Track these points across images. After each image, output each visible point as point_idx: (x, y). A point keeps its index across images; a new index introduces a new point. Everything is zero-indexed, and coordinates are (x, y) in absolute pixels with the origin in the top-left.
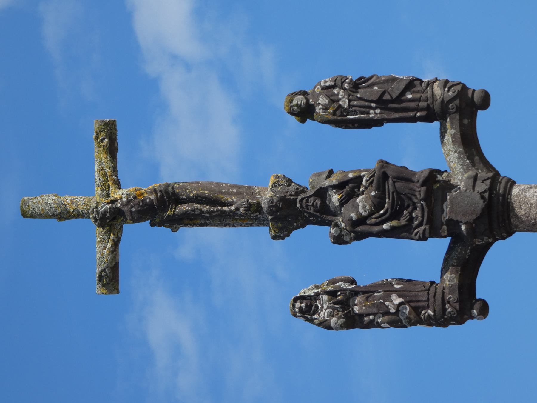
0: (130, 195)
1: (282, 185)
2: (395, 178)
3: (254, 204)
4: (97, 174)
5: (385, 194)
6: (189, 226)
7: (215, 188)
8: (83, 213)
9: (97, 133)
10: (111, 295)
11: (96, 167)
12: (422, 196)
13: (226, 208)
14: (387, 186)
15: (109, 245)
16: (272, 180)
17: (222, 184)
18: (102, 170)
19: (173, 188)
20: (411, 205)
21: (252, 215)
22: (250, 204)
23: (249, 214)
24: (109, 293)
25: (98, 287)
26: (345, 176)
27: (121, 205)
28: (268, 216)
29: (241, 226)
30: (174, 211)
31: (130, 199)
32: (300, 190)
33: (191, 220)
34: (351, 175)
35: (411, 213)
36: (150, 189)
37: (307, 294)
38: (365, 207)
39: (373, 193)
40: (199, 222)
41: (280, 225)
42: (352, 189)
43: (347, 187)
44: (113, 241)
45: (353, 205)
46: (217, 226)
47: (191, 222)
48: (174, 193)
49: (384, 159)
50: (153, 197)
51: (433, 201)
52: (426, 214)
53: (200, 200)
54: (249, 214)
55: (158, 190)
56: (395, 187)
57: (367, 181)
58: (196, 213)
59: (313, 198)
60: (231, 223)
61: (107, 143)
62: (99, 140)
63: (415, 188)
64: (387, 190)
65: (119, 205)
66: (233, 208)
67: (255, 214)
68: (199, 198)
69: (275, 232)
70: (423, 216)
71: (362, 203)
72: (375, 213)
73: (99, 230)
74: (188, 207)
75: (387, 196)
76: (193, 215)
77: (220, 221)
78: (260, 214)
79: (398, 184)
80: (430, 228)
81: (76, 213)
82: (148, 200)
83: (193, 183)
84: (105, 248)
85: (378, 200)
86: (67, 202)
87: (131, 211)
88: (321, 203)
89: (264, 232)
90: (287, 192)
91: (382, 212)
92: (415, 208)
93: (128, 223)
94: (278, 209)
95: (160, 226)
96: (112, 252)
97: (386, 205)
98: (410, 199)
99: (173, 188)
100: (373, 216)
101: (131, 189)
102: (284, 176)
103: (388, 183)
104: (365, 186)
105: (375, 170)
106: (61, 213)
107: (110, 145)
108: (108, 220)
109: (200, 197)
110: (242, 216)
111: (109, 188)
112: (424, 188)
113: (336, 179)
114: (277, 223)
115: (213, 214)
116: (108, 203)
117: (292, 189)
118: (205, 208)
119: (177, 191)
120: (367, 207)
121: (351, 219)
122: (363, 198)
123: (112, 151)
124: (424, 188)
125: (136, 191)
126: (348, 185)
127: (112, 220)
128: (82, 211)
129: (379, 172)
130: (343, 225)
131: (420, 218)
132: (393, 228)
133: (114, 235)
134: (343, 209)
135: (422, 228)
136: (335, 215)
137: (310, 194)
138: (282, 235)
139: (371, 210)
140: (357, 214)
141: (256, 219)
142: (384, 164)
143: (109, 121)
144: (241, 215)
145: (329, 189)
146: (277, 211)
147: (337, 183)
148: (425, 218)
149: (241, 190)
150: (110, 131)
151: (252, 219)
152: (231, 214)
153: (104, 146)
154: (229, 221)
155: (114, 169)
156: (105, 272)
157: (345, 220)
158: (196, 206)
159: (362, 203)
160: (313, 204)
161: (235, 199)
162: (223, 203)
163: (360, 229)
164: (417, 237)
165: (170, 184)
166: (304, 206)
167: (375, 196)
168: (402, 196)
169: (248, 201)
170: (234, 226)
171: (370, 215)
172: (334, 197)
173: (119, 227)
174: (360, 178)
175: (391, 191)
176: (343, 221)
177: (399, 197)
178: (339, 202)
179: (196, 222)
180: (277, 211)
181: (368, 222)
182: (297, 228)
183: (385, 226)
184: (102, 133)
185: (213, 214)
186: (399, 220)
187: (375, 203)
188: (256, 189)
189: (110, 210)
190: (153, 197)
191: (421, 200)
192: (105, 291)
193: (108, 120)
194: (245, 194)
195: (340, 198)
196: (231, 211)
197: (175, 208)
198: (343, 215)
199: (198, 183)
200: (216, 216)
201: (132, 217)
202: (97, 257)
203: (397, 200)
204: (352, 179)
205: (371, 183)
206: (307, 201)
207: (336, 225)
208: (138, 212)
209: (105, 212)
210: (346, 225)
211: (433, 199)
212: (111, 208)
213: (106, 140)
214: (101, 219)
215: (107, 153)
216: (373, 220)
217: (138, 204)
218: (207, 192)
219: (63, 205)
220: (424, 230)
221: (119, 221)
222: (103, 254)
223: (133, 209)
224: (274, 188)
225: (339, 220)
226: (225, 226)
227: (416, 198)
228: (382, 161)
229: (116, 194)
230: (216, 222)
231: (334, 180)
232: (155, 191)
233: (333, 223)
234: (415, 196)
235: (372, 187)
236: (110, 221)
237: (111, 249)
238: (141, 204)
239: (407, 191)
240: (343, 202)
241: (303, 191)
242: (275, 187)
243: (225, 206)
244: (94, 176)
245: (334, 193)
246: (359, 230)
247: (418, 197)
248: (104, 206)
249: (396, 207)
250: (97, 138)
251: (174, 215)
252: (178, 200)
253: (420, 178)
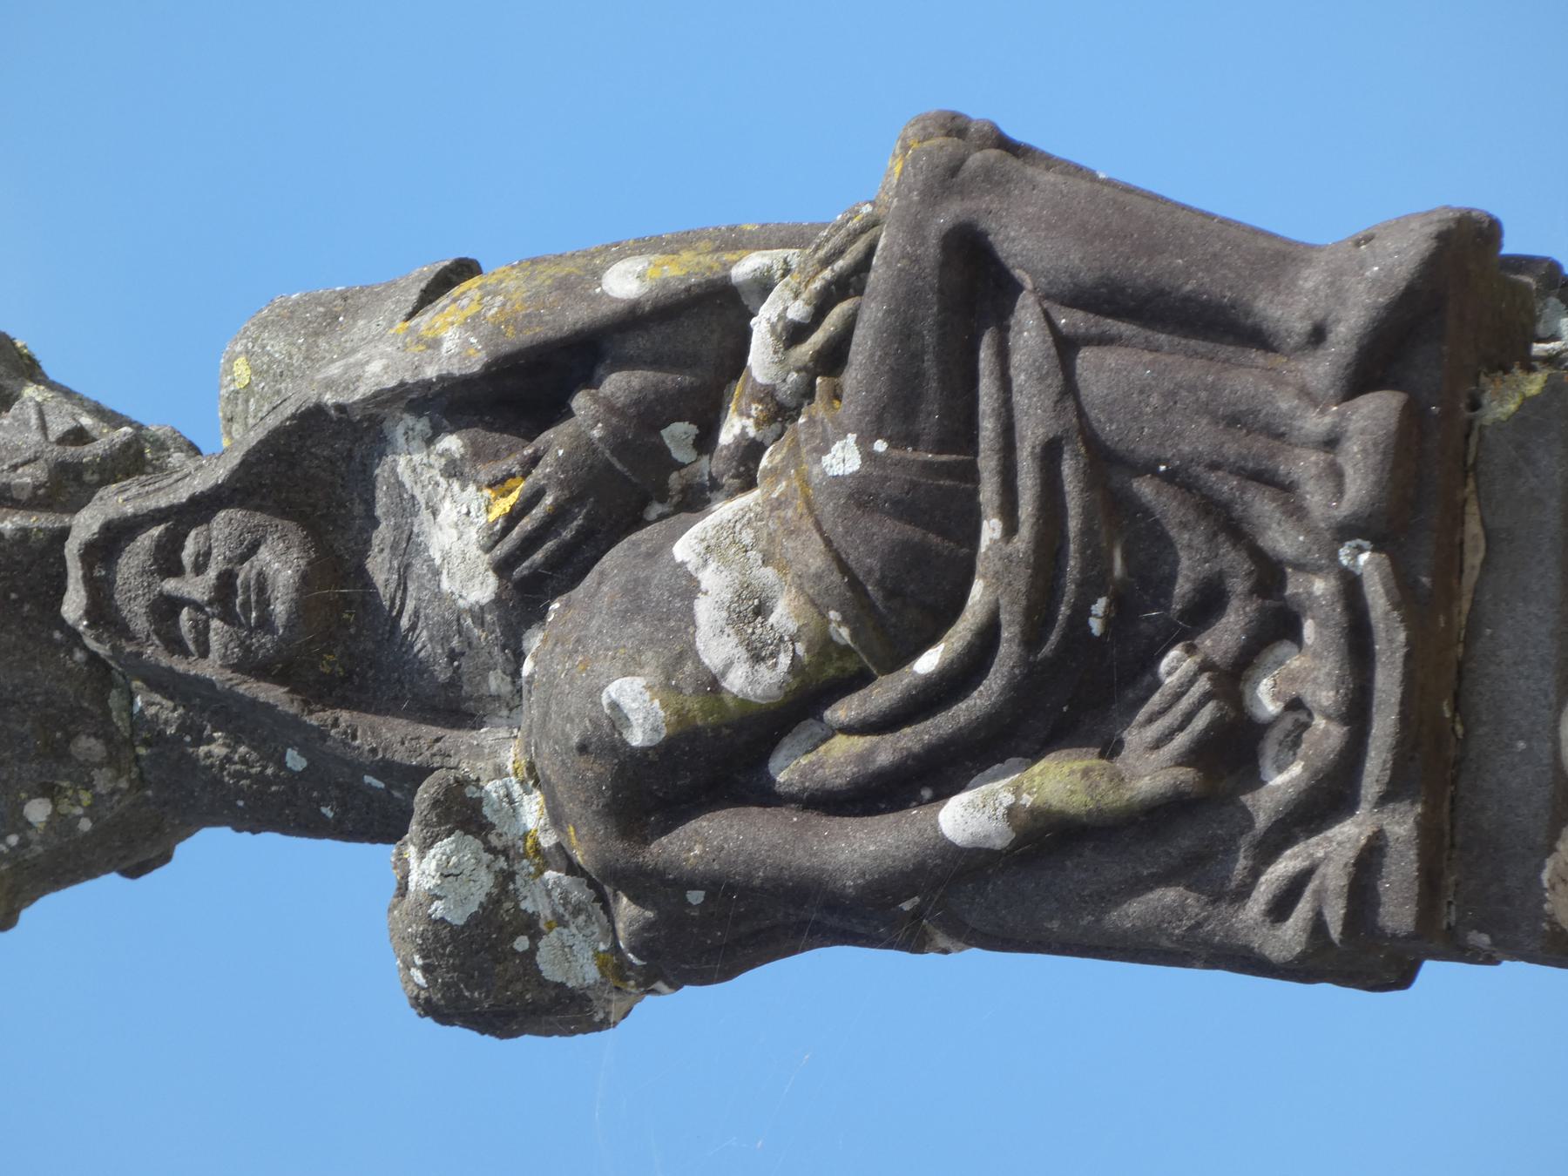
2: (1078, 299)
5: (970, 473)
12: (1358, 488)
14: (987, 386)
20: (1238, 585)
26: (565, 286)
32: (98, 448)
34: (624, 283)
35: (1231, 680)
38: (761, 610)
39: (844, 459)
42: (648, 416)
43: (581, 402)
45: (635, 603)
49: (978, 110)
51: (1474, 559)
52: (1387, 683)
56: (1070, 388)
57: (794, 334)
59: (224, 525)
63: (1285, 402)
64: (988, 427)
70: (1356, 712)
71: (732, 583)
72: (860, 680)
75: (988, 492)
79: (1111, 357)
80: (1435, 845)
85: (889, 530)
88: (305, 581)
91: (928, 662)
92: (1280, 626)
97: (978, 590)
98: (1229, 525)
100: (843, 711)
103: (1003, 354)
104: (767, 394)
105: (873, 223)
112: (1376, 412)
113: (472, 324)
118: (840, 264)
120: (784, 615)
121: (603, 743)
122: (741, 518)
124: (1376, 412)
126: (589, 380)
129: (916, 230)
130: (532, 812)
131: (1326, 734)
132: (1044, 838)
134: (534, 641)
135: (1349, 833)
136: (456, 708)
137: (199, 484)
139: (825, 647)
140: (667, 687)
142: (970, 155)
145: (404, 426)
147: (475, 361)
148: (1384, 726)
157: (547, 767)
159: (732, 583)
160: (226, 581)
163: (708, 840)
164: (1290, 936)
166: (137, 615)
167: (861, 494)
168: (1145, 488)
171: (802, 705)
172: (448, 512)
174: (717, 310)
175: (1030, 435)
176: (533, 776)
177: (1115, 507)
178: (502, 568)
181: (789, 769)
183: (966, 816)
186: (1111, 749)
187: (865, 561)
191: (1346, 531)
195: (512, 518)
198: (531, 710)
203: (1087, 531)
204: (633, 320)
205: (833, 358)
206: (167, 561)
207: (463, 812)
210: (556, 818)
211: (1473, 527)
216: (839, 757)
220: (1370, 858)
225: (496, 759)
227: (1296, 511)
228: (955, 126)
231: (455, 341)
233: (425, 794)
234: (1285, 489)
235: (836, 395)
239: (1197, 438)
240: (537, 575)
241: (134, 459)
245: (453, 470)
246: (694, 871)
247: (1315, 498)
249: (1081, 612)
253: (1338, 294)
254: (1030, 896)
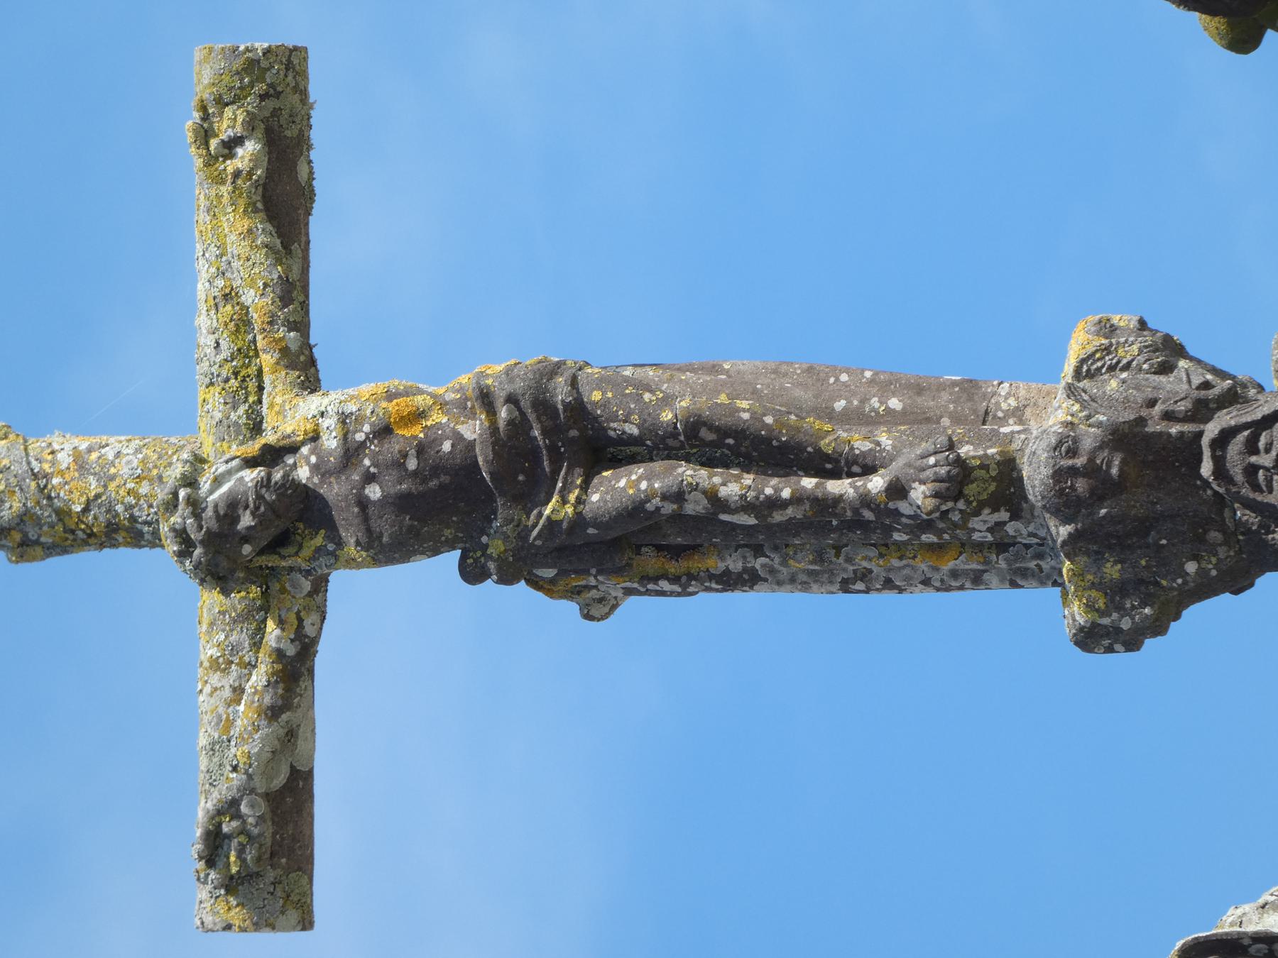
0: (360, 420)
1: (1127, 367)
3: (982, 466)
4: (204, 321)
6: (665, 585)
7: (798, 393)
8: (133, 519)
9: (203, 108)
10: (266, 936)
11: (202, 287)
13: (839, 487)
15: (258, 678)
16: (1079, 342)
17: (836, 371)
18: (227, 297)
19: (574, 382)
21: (975, 523)
22: (959, 462)
23: (956, 517)
24: (257, 927)
25: (203, 893)
27: (315, 469)
28: (1052, 522)
29: (926, 582)
30: (579, 501)
31: (360, 437)
33: (677, 552)
36: (461, 389)
37: (1250, 928)
40: (716, 564)
41: (1112, 571)
44: (279, 654)
46: (805, 587)
47: (673, 567)
48: (578, 409)
50: (472, 429)
53: (712, 444)
54: (956, 517)
55: (500, 396)
58: (690, 509)
60: (876, 567)
61: (255, 159)
62: (214, 143)
65: (303, 474)
66: (876, 483)
67: (989, 517)
68: (705, 434)
69: (1090, 607)
73: (211, 600)
74: (649, 477)
76: (678, 518)
77: (820, 557)
78: (1015, 516)
81: (97, 518)
82: (447, 446)
83: (690, 368)
84: (238, 691)
86: (53, 463)
87: (363, 503)
89: (1045, 614)
90: (1152, 403)
93: (351, 563)
94: (1105, 488)
95: (506, 579)
96: (273, 713)
99: (574, 382)
101: (366, 389)
102: (1143, 325)
106: (24, 517)
107: (270, 174)
108: (247, 549)
109: (711, 428)
110: (927, 525)
111: (261, 388)
114: (1098, 558)
115: (778, 517)
116: (250, 463)
117: (1178, 386)
118: (735, 485)
119: (596, 396)
123: (282, 202)
125: (390, 396)
127: (269, 546)
128: (129, 507)
133: (281, 623)
138: (1126, 624)
141: (1002, 546)
143: (267, 52)
144: (922, 524)
146: (1098, 497)
149: (925, 402)
150: (271, 104)
151: (980, 547)
152: (868, 515)
153: (237, 174)
154: (865, 559)
155: (293, 293)
156: (237, 816)
158: (687, 472)
161: (886, 440)
162: (827, 458)
165: (559, 365)
166: (1237, 473)
169: (951, 446)
170: (888, 584)
173: (307, 585)
179: (695, 564)
180: (1098, 497)
182: (1204, 589)
184: (228, 112)
185: (778, 517)
188: (1005, 396)
189: (259, 497)
190: (472, 429)
192: (237, 916)
193: (261, 45)
194: (946, 421)
196: (866, 500)
197: (585, 487)
199: (714, 369)
200: (792, 527)
201: (369, 531)
202: (203, 741)
208: (401, 503)
209: (233, 506)
212: (265, 483)
213: (250, 148)
214: (211, 540)
215: (251, 209)
217: (399, 464)
218: (744, 404)
219: (35, 476)
221: (307, 552)
222: (230, 723)
223: (374, 492)
224: (1085, 384)
226: (846, 587)
229: (289, 413)
230: (801, 564)
232: (485, 398)
236: (261, 552)
237: (267, 700)
238: (412, 464)
241: (1233, 397)
242: (1091, 375)
243: (836, 475)
244: (193, 331)
248: (229, 473)
250: (204, 134)
251: (579, 521)
252: (598, 448)
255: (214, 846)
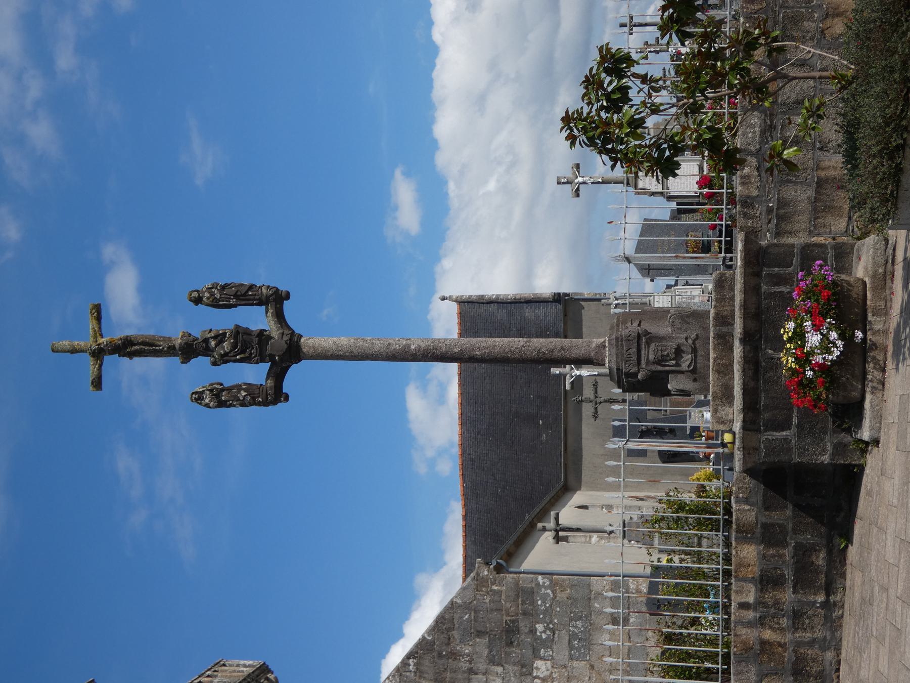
89: (177, 360)
117: (191, 338)
123: (99, 319)
127: (98, 354)
142: (237, 326)
155: (100, 328)
171: (230, 352)
229: (101, 340)
231: (212, 334)
240: (217, 345)
254: (241, 361)
255: (92, 383)
